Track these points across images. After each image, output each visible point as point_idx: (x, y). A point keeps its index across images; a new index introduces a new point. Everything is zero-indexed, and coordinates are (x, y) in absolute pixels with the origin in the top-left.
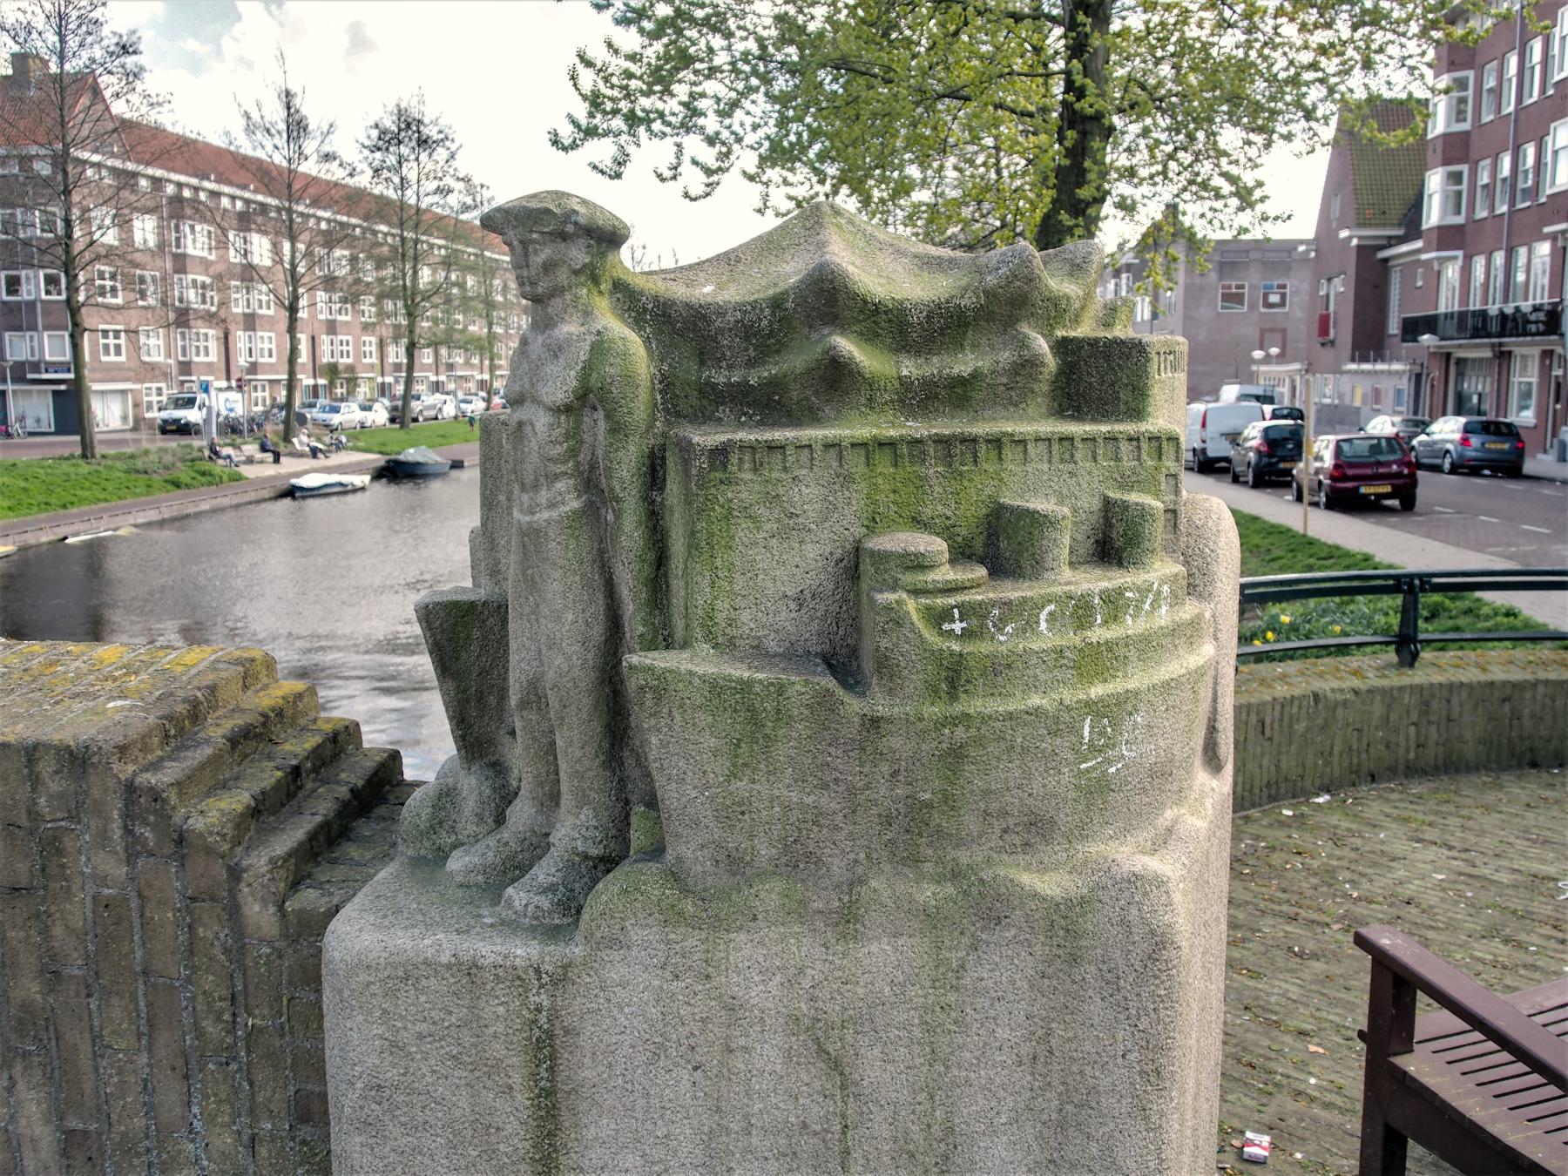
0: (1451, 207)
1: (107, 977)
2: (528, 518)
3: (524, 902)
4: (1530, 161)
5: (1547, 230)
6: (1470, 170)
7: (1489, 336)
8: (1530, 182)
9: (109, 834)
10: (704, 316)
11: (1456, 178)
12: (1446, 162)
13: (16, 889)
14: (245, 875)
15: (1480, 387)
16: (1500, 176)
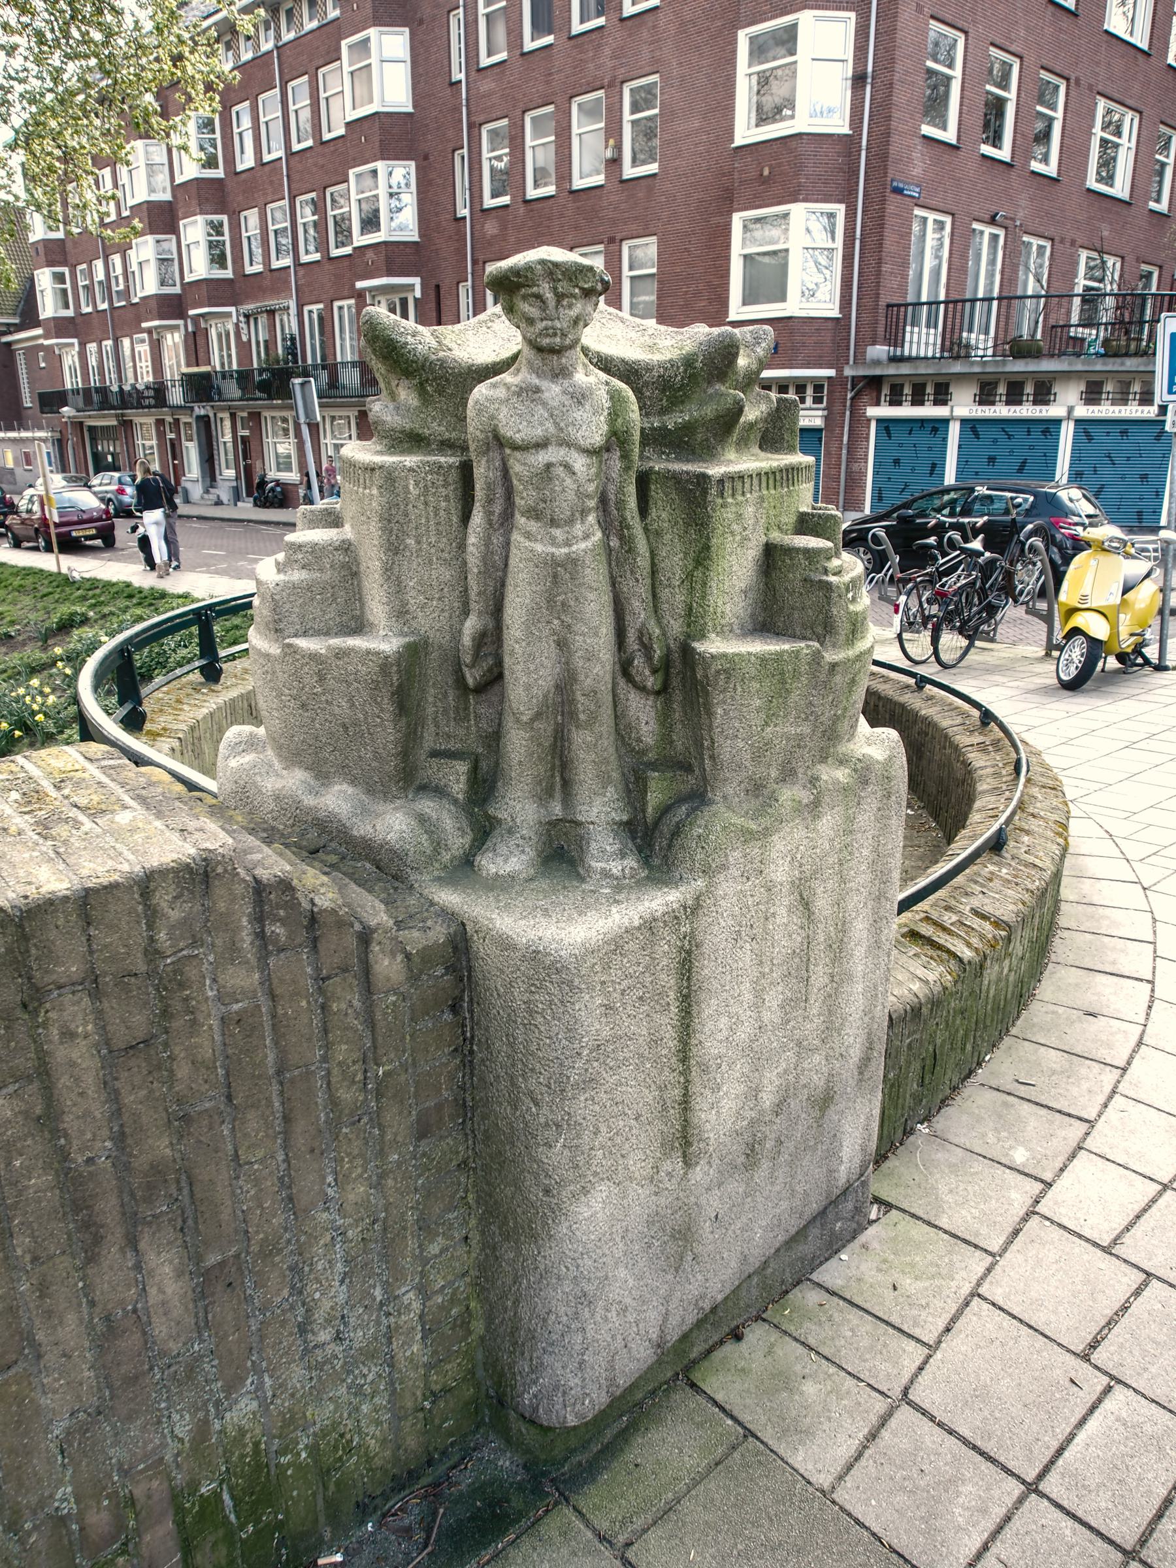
0: (60, 304)
1: (241, 1095)
2: (565, 550)
3: (620, 868)
4: (119, 270)
5: (144, 325)
6: (70, 272)
7: (114, 408)
8: (121, 287)
9: (239, 945)
10: (637, 371)
11: (60, 278)
12: (50, 264)
13: (132, 1047)
14: (375, 935)
15: (111, 449)
16: (96, 280)
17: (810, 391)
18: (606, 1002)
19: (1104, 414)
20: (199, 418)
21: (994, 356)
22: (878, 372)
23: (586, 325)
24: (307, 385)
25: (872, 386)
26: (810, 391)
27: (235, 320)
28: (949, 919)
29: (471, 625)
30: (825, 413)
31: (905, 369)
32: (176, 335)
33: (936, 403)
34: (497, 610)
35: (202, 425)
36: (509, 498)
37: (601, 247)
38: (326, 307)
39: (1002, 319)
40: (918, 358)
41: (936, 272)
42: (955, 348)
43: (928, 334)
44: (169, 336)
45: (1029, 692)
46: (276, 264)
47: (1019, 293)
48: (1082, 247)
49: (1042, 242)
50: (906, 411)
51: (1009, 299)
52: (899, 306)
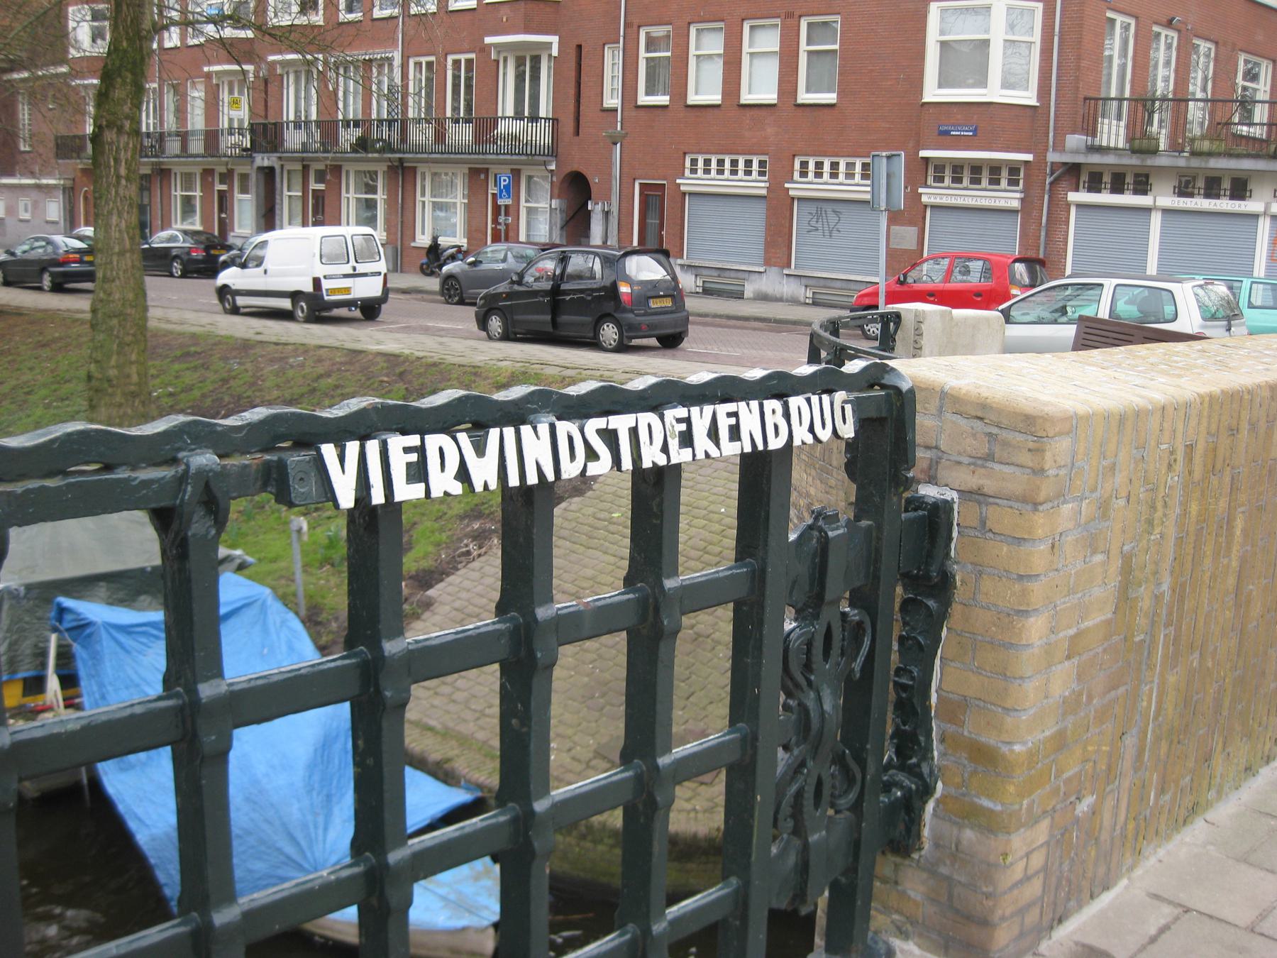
17: (1005, 174)
19: (1218, 207)
20: (261, 169)
24: (895, 159)
25: (1072, 173)
26: (1005, 174)
30: (1022, 195)
33: (1090, 190)
35: (262, 177)
37: (778, 21)
41: (1123, 68)
42: (1141, 144)
45: (255, 601)
48: (1241, 50)
49: (1209, 45)
50: (1105, 198)
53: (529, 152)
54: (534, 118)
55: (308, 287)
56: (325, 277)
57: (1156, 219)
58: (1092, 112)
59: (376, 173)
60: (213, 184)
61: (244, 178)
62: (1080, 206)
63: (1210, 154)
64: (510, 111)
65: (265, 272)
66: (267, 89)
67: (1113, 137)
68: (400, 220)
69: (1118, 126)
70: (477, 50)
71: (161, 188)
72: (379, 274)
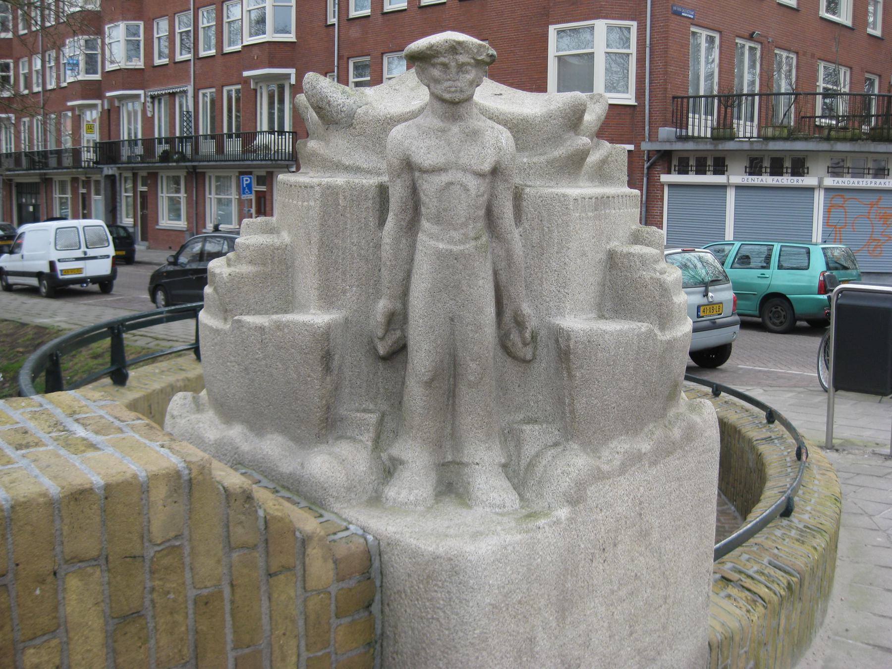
5: (69, 104)
16: (34, 69)
18: (493, 602)
20: (107, 176)
21: (758, 137)
22: (667, 147)
23: (478, 86)
27: (142, 100)
28: (752, 569)
29: (382, 306)
31: (690, 146)
32: (94, 112)
33: (716, 172)
34: (405, 294)
36: (417, 209)
38: (217, 90)
39: (763, 110)
40: (699, 137)
43: (706, 120)
44: (88, 113)
46: (179, 58)
47: (775, 91)
51: (768, 95)
52: (682, 98)
53: (276, 158)
54: (281, 132)
55: (46, 269)
56: (59, 260)
57: (731, 195)
58: (679, 108)
59: (179, 177)
60: (78, 188)
61: (97, 182)
62: (672, 186)
63: (774, 139)
64: (265, 128)
65: (22, 257)
66: (110, 117)
67: (703, 129)
68: (194, 212)
69: (752, 126)
70: (242, 82)
71: (46, 192)
72: (108, 257)
